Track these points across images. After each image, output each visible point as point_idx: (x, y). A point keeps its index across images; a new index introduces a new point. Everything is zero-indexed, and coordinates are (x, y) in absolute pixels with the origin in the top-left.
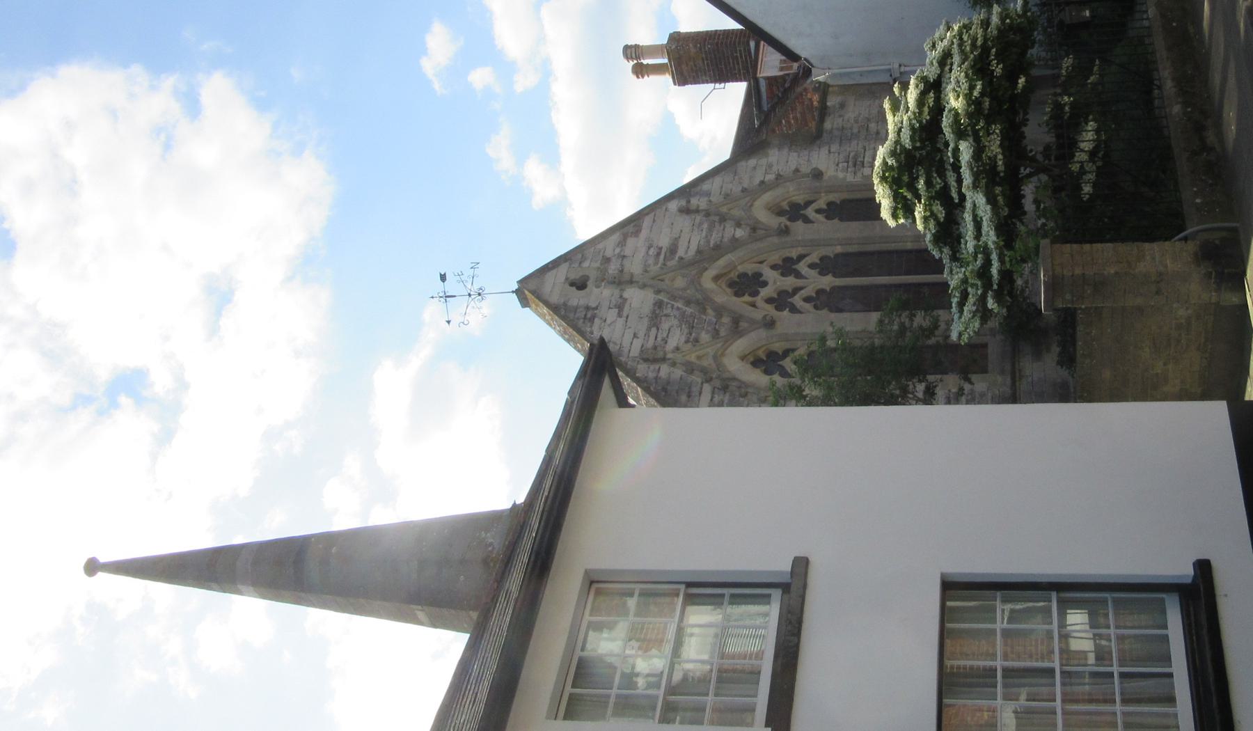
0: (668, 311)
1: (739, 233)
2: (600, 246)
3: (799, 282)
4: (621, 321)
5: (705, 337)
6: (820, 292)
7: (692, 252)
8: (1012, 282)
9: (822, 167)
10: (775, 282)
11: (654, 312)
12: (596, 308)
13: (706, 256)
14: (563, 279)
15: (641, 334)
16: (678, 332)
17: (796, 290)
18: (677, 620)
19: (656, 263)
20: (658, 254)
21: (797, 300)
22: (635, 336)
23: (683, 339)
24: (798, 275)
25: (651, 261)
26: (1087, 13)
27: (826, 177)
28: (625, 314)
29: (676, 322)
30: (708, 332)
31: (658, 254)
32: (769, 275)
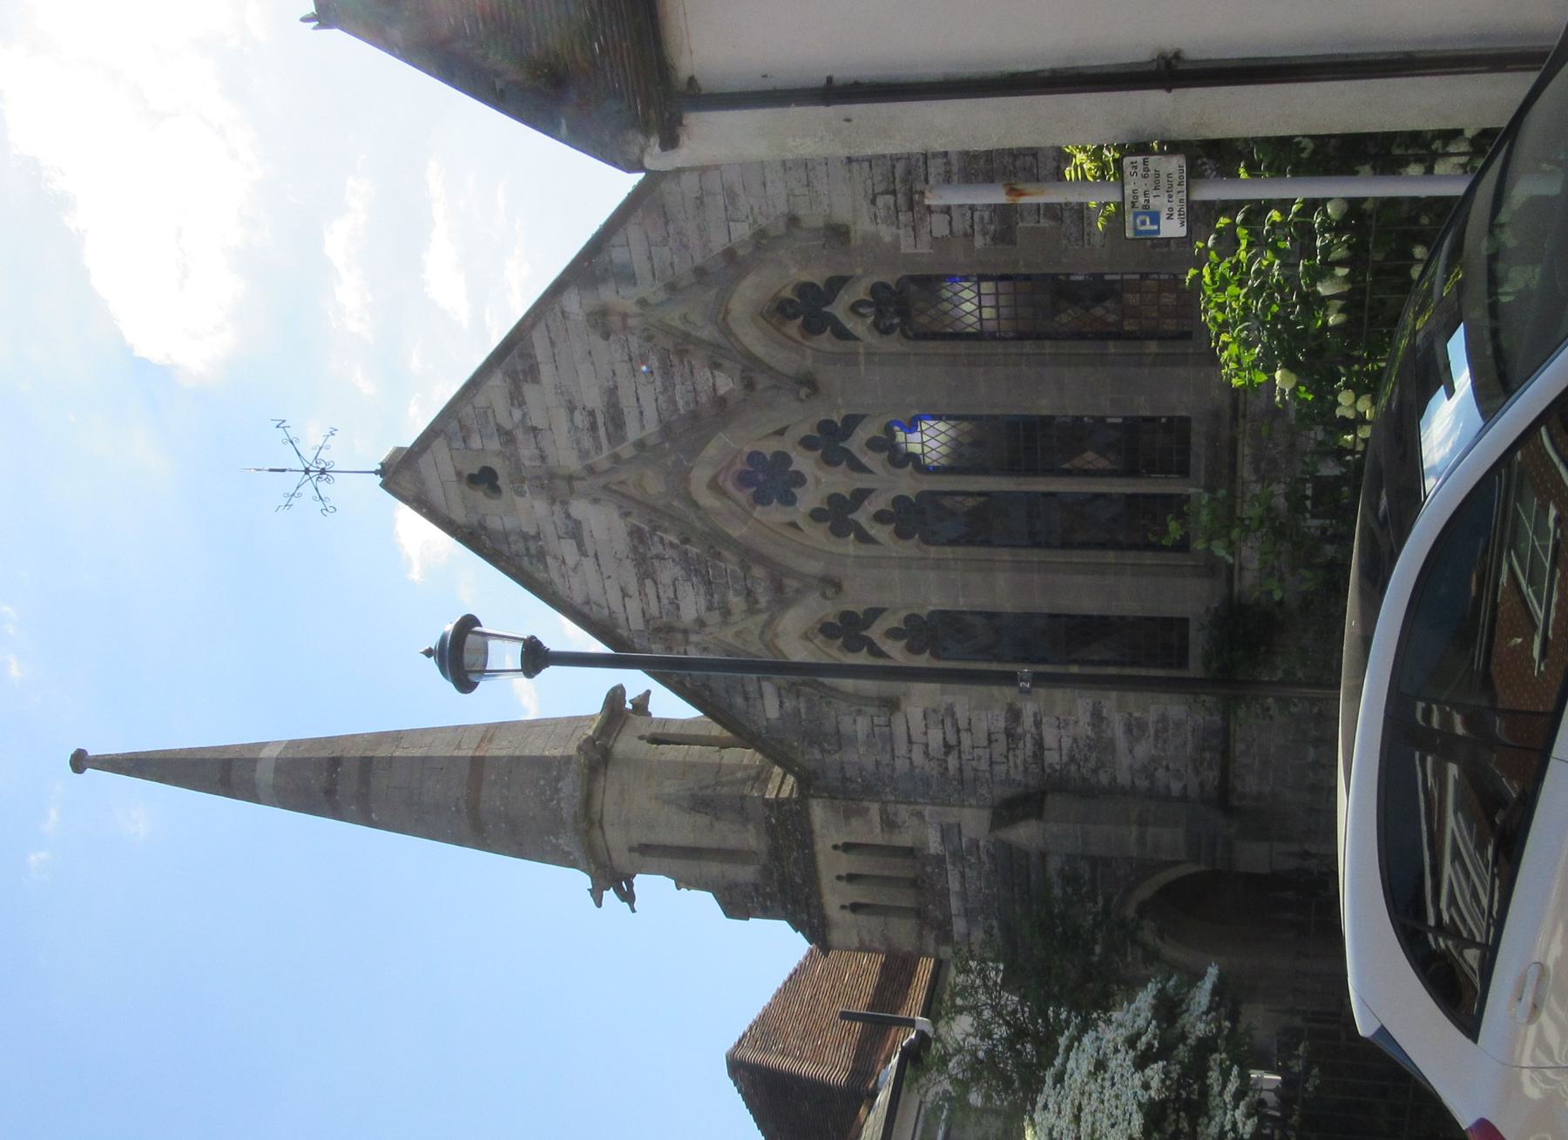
0: (657, 549)
1: (725, 384)
2: (481, 401)
3: (861, 481)
4: (588, 564)
5: (736, 602)
6: (899, 501)
7: (652, 427)
8: (1100, 711)
9: (842, 214)
10: (818, 481)
11: (635, 549)
12: (537, 537)
13: (689, 429)
14: (450, 474)
15: (633, 588)
16: (688, 588)
17: (861, 496)
18: (877, 872)
19: (599, 448)
20: (593, 427)
21: (862, 517)
22: (625, 594)
23: (703, 603)
24: (857, 466)
25: (587, 443)
26: (1345, 489)
27: (856, 240)
28: (591, 553)
29: (678, 571)
30: (737, 593)
31: (593, 427)
32: (804, 462)
